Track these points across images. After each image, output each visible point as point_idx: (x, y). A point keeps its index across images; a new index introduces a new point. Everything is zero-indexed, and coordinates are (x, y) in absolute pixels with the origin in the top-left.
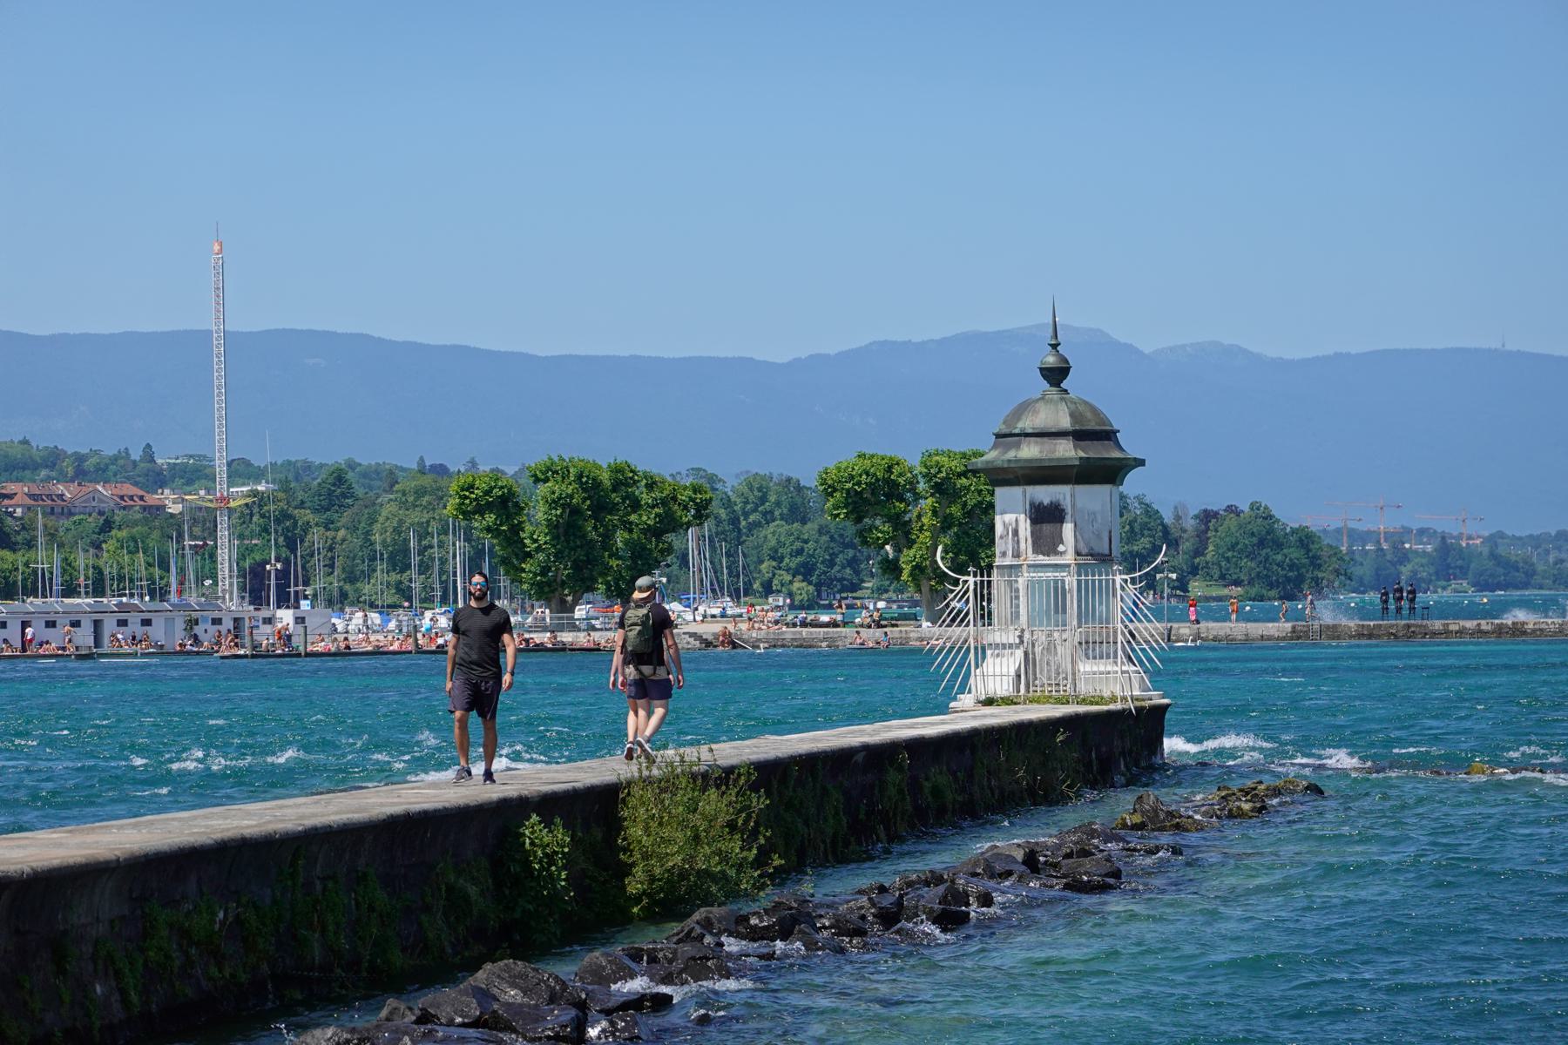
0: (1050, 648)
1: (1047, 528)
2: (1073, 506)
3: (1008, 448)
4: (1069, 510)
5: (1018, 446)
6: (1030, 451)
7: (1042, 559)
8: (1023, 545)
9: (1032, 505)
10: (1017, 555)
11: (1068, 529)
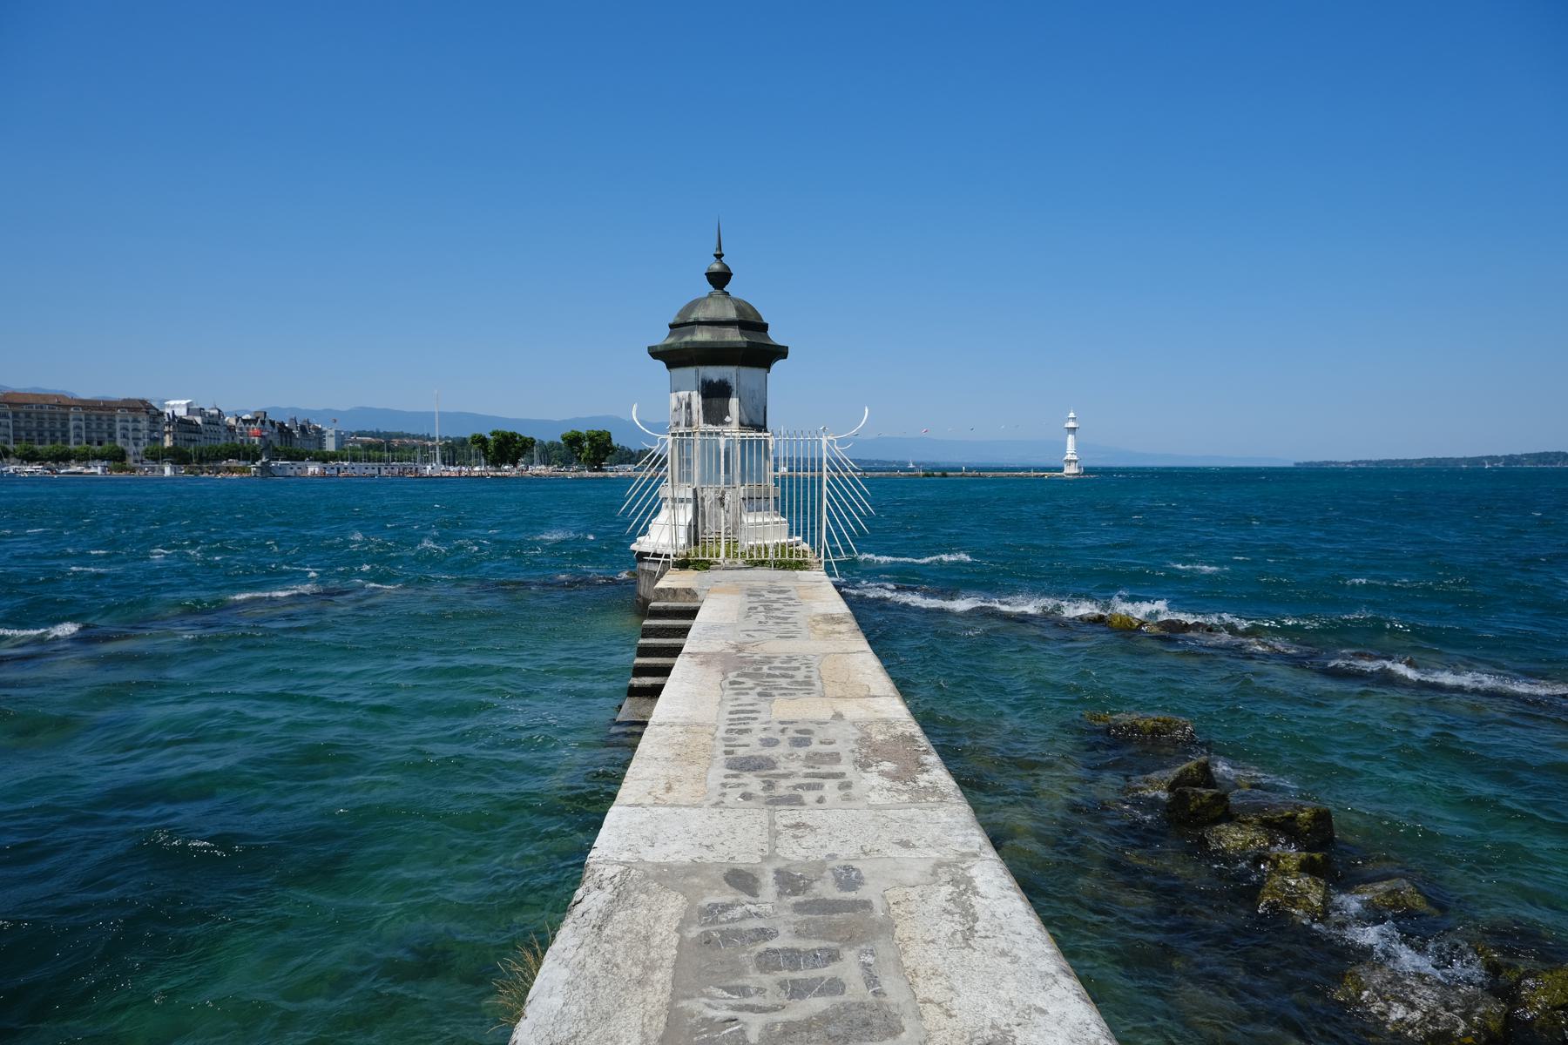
1: (716, 402)
3: (683, 334)
5: (692, 333)
6: (703, 336)
7: (711, 428)
8: (695, 416)
9: (704, 382)
10: (689, 424)
11: (734, 403)
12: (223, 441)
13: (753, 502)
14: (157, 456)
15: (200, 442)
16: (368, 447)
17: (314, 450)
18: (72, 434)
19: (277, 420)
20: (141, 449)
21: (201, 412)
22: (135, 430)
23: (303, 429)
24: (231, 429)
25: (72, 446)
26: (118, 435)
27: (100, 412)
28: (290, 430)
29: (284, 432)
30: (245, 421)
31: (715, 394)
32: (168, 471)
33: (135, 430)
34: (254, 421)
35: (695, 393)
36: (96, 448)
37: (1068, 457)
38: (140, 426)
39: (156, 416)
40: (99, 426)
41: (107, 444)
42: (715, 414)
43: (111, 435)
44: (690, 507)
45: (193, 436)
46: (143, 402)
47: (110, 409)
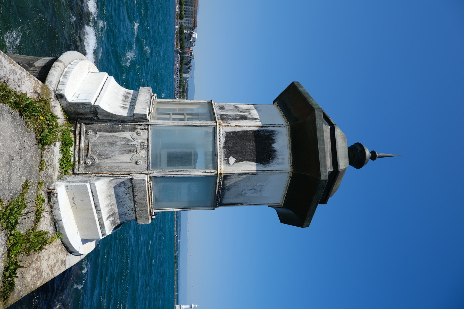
0: (130, 149)
1: (251, 146)
2: (272, 172)
4: (268, 168)
7: (221, 140)
8: (234, 123)
9: (272, 133)
10: (223, 118)
11: (250, 167)
12: (185, 46)
13: (126, 189)
14: (181, 27)
15: (185, 39)
16: (184, 86)
17: (183, 71)
18: (187, 7)
19: (192, 61)
20: (183, 24)
21: (194, 41)
22: (189, 23)
23: (189, 68)
24: (189, 48)
25: (184, 6)
26: (187, 19)
27: (194, 14)
28: (188, 64)
29: (188, 63)
30: (191, 53)
31: (259, 146)
32: (177, 27)
33: (189, 23)
34: (191, 55)
35: (260, 124)
36: (183, 13)
37: (182, 306)
38: (189, 24)
39: (193, 28)
40: (190, 14)
41: (184, 15)
42: (237, 145)
43: (187, 17)
44: (124, 113)
45: (187, 38)
46: (196, 26)
47: (194, 18)
